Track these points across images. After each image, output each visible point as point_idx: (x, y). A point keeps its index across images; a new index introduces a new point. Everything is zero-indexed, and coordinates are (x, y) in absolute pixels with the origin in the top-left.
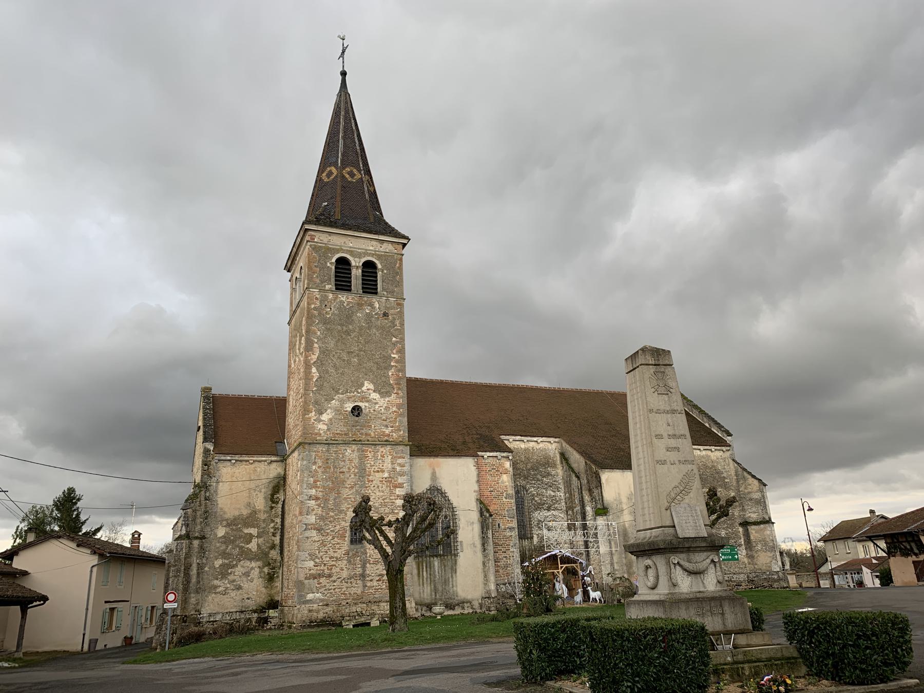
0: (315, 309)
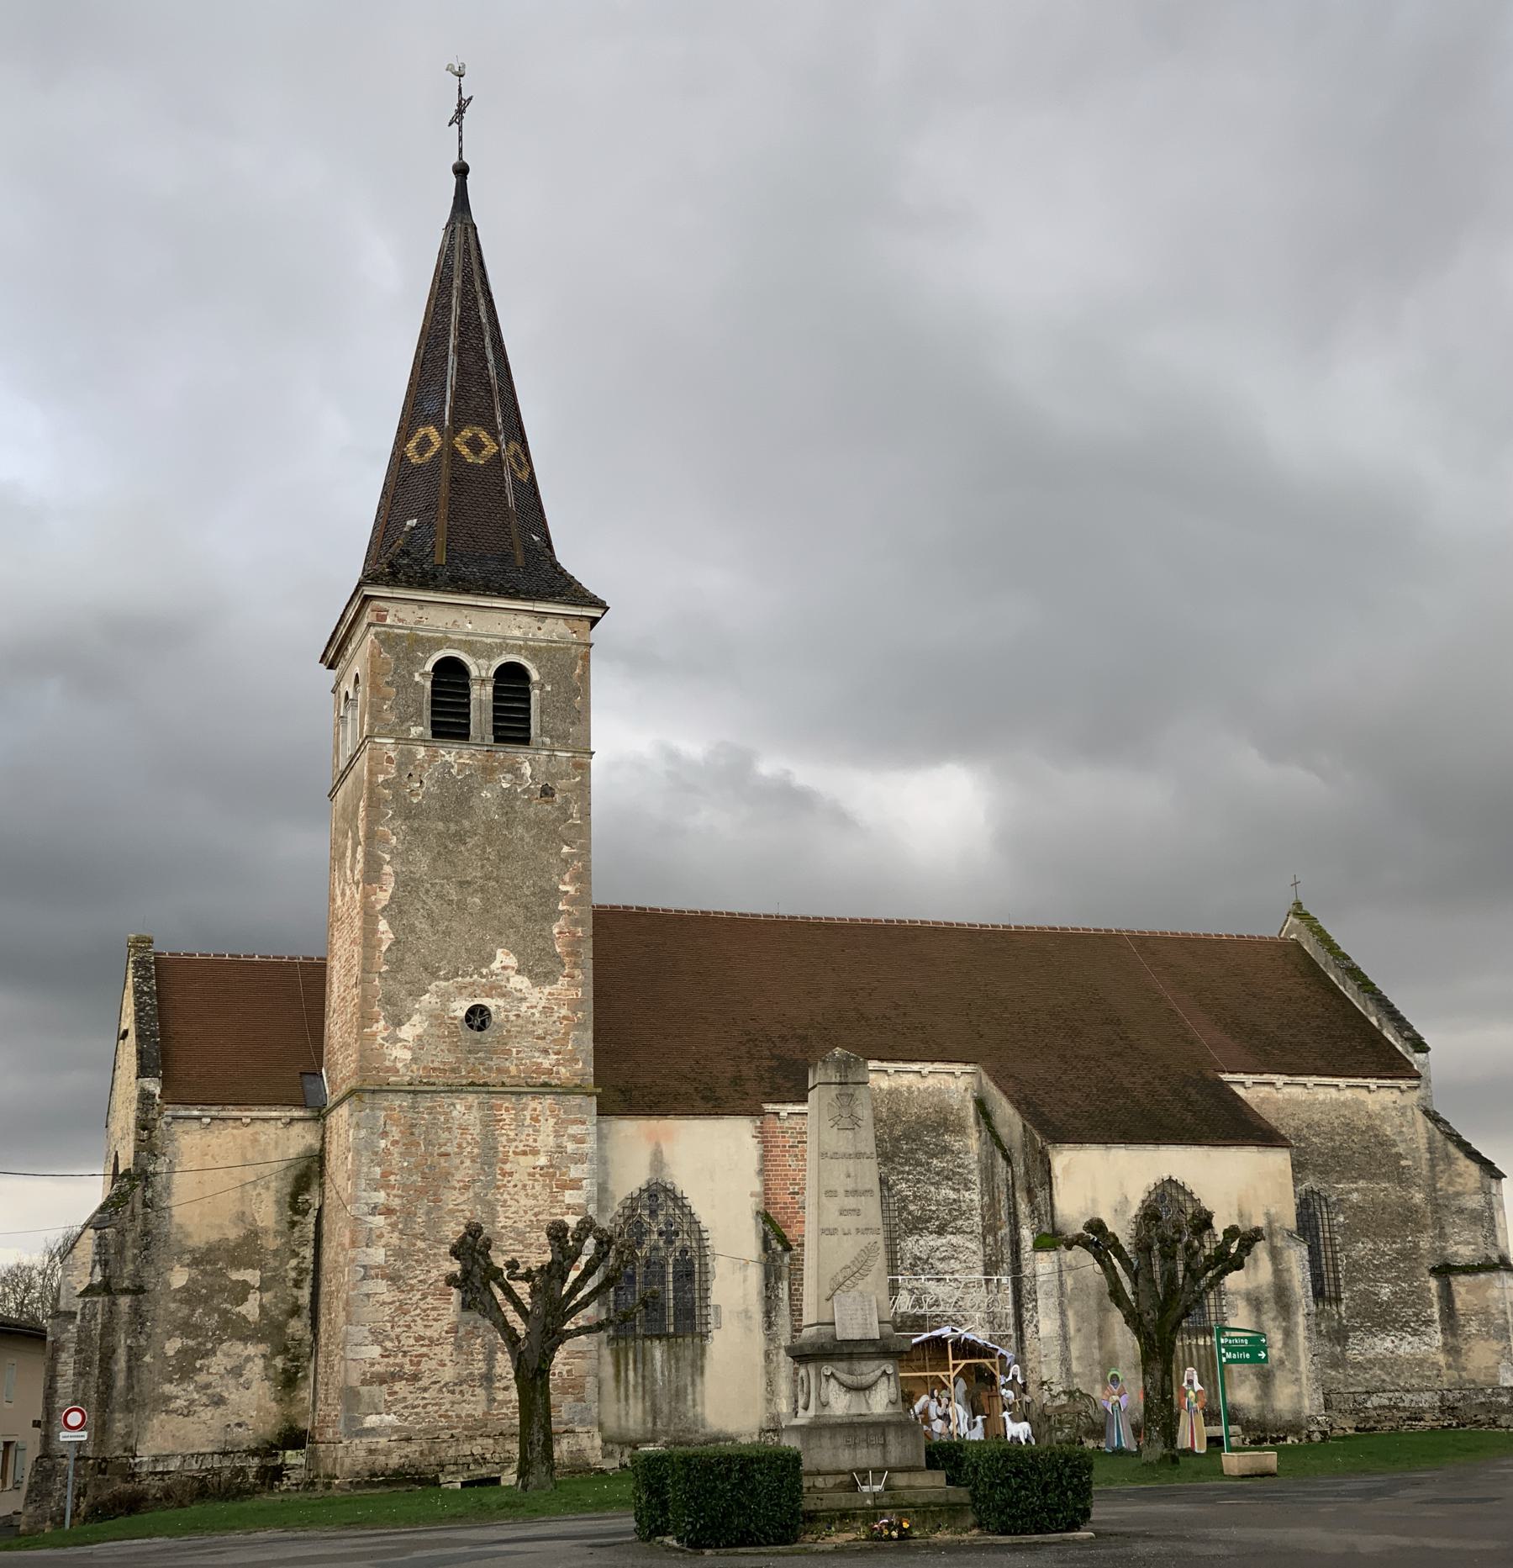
0: (387, 784)
